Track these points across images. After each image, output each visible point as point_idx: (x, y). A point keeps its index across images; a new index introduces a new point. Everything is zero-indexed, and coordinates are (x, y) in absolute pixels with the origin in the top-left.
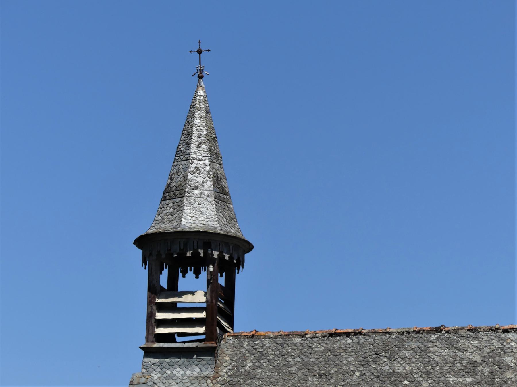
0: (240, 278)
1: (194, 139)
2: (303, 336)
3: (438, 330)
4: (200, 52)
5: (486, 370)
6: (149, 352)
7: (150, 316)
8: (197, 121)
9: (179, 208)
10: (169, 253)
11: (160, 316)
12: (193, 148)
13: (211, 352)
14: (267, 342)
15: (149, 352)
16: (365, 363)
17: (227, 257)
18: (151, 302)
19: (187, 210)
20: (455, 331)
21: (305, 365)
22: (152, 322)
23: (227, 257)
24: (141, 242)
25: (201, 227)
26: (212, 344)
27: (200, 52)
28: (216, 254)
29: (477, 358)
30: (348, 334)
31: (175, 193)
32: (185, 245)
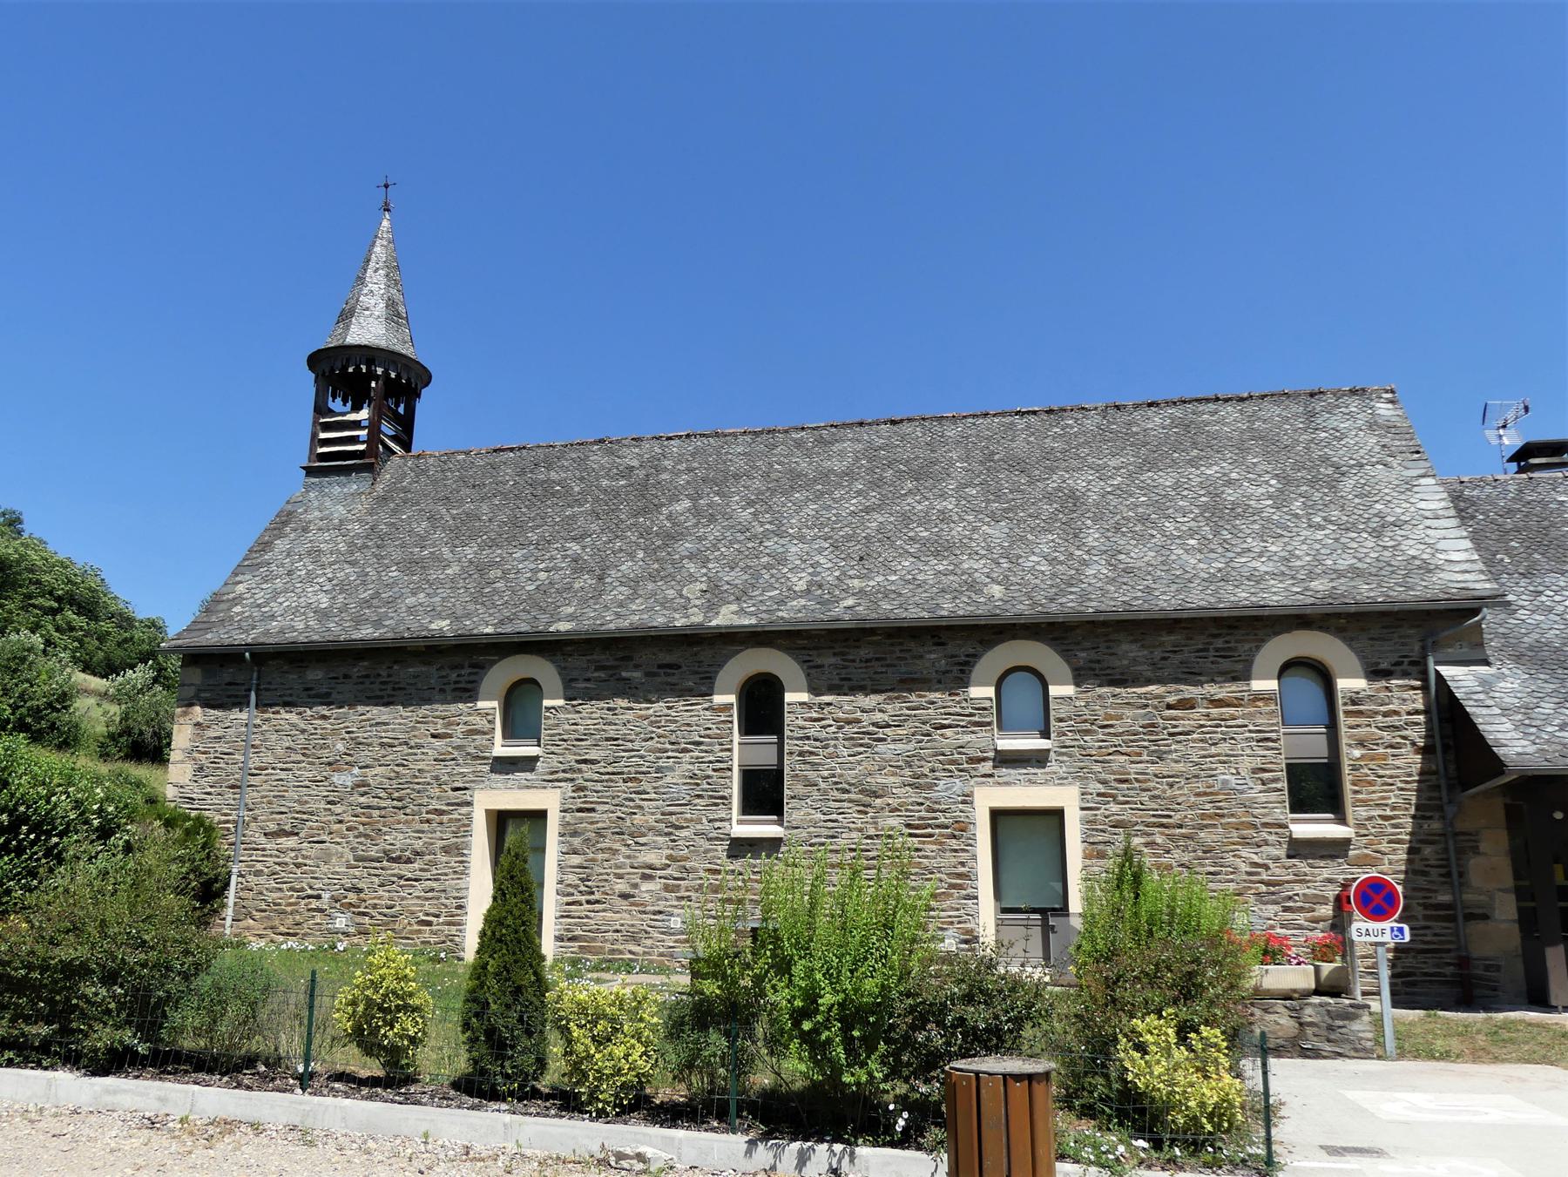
0: (421, 407)
1: (372, 264)
2: (467, 453)
3: (602, 441)
4: (386, 186)
5: (642, 473)
6: (310, 471)
7: (314, 435)
8: (377, 249)
9: (347, 328)
10: (343, 373)
11: (323, 436)
12: (370, 272)
13: (369, 468)
14: (431, 461)
15: (310, 471)
16: (522, 473)
17: (393, 375)
18: (315, 422)
19: (354, 328)
20: (618, 442)
21: (461, 478)
22: (316, 442)
23: (393, 375)
24: (315, 360)
25: (364, 342)
26: (1390, 1044)
27: (386, 186)
28: (380, 371)
29: (635, 463)
30: (511, 450)
31: (346, 316)
32: (348, 360)
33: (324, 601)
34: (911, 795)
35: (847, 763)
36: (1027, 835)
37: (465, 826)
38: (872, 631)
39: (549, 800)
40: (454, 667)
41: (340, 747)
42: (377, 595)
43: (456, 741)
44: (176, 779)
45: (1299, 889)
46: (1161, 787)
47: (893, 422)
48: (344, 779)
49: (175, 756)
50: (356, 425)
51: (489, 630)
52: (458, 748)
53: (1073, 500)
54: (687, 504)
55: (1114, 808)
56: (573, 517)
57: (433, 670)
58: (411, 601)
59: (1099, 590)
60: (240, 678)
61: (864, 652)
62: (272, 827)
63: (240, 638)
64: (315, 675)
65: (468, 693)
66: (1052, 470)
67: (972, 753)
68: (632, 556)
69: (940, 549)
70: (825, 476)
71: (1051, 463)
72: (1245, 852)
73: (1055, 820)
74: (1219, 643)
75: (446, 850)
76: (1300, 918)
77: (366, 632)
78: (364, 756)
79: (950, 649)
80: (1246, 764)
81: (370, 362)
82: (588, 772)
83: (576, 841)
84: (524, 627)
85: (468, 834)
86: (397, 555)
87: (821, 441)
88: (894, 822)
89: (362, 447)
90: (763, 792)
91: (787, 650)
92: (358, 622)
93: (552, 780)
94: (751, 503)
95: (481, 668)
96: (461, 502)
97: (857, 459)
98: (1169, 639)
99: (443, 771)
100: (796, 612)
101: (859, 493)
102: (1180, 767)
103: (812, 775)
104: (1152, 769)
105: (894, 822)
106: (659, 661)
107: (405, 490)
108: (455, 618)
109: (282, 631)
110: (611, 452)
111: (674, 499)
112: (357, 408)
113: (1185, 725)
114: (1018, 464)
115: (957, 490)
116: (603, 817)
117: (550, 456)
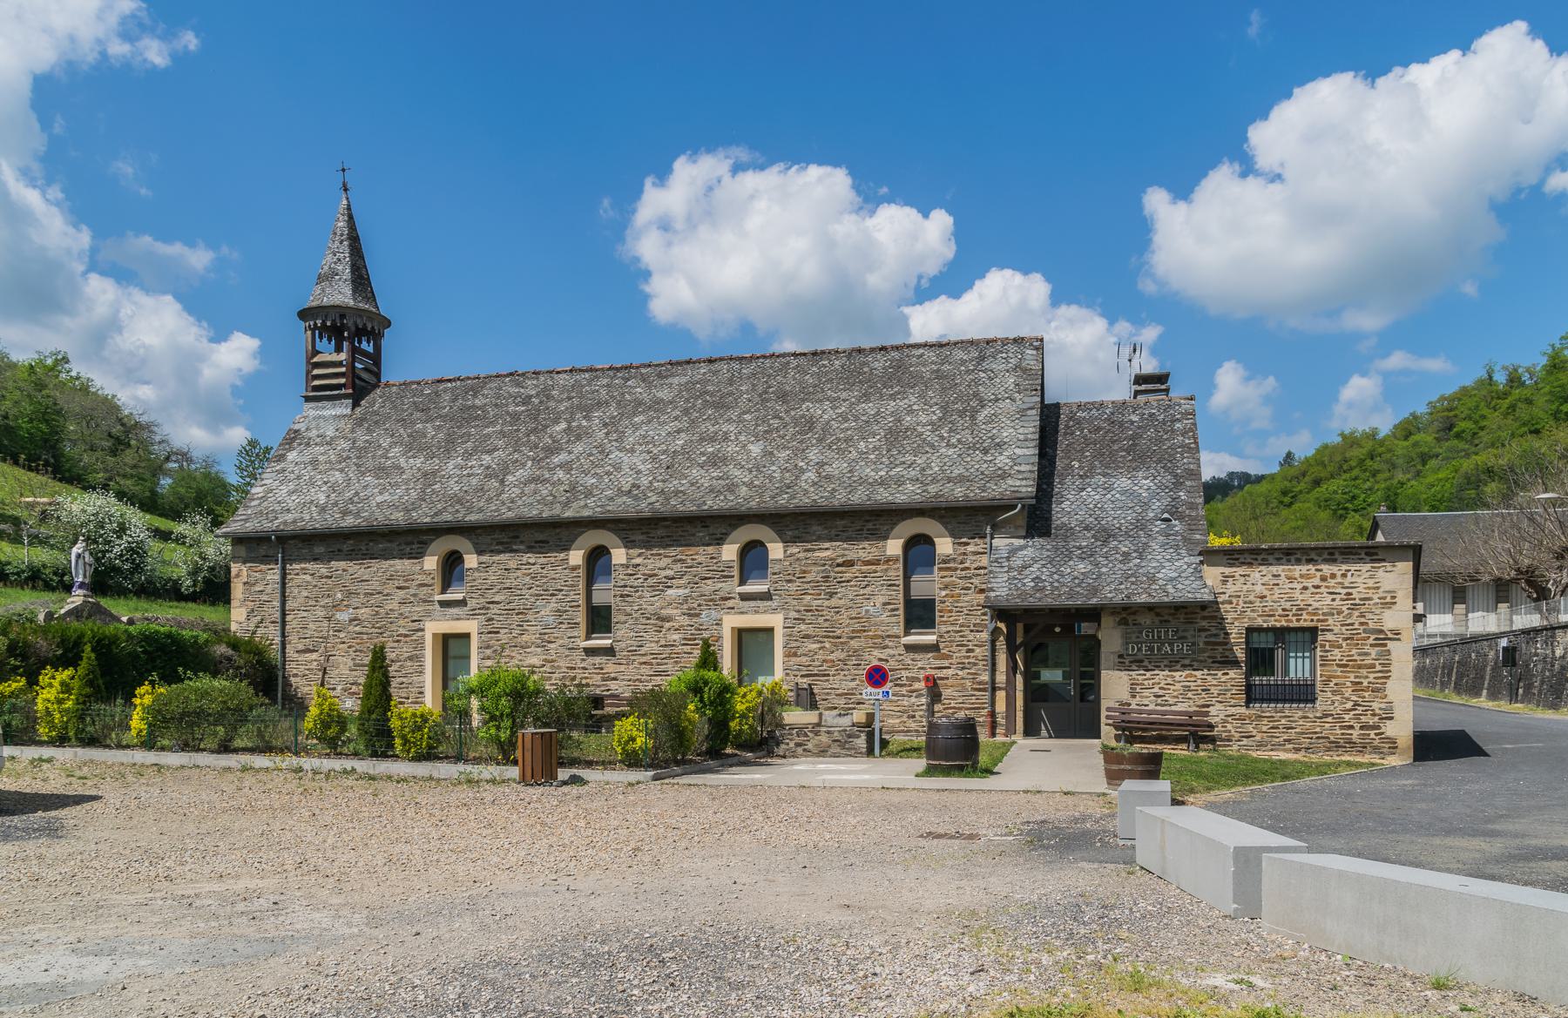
7: (308, 372)
11: (316, 372)
15: (308, 399)
33: (322, 499)
34: (685, 621)
35: (650, 602)
36: (451, 648)
37: (420, 644)
38: (665, 519)
39: (471, 626)
40: (408, 544)
41: (339, 596)
42: (357, 494)
43: (412, 591)
44: (238, 618)
45: (905, 674)
46: (829, 615)
47: (710, 361)
48: (343, 616)
49: (234, 603)
50: (340, 364)
51: (428, 520)
52: (414, 595)
53: (810, 423)
54: (563, 425)
55: (803, 627)
56: (488, 436)
57: (394, 545)
58: (379, 499)
59: (808, 493)
60: (271, 552)
61: (660, 532)
62: (301, 647)
63: (267, 526)
64: (319, 549)
65: (419, 555)
66: (804, 400)
67: (721, 594)
68: (524, 465)
69: (715, 461)
70: (659, 401)
71: (807, 394)
72: (876, 653)
73: (452, 642)
74: (870, 526)
75: (410, 658)
76: (904, 690)
77: (349, 521)
78: (355, 601)
79: (711, 530)
80: (880, 600)
81: (343, 316)
82: (495, 609)
83: (488, 652)
84: (449, 517)
85: (423, 648)
86: (370, 464)
87: (660, 376)
88: (676, 637)
89: (343, 381)
90: (599, 619)
91: (616, 531)
92: (345, 513)
93: (473, 615)
94: (605, 425)
95: (426, 544)
96: (413, 423)
97: (680, 391)
98: (840, 523)
99: (406, 609)
100: (623, 506)
101: (676, 418)
102: (842, 602)
103: (628, 609)
104: (827, 603)
105: (676, 637)
106: (545, 534)
107: (376, 413)
108: (407, 511)
109: (295, 521)
110: (518, 385)
111: (556, 421)
112: (339, 349)
113: (848, 576)
114: (783, 396)
115: (739, 416)
116: (504, 636)
117: (476, 384)
